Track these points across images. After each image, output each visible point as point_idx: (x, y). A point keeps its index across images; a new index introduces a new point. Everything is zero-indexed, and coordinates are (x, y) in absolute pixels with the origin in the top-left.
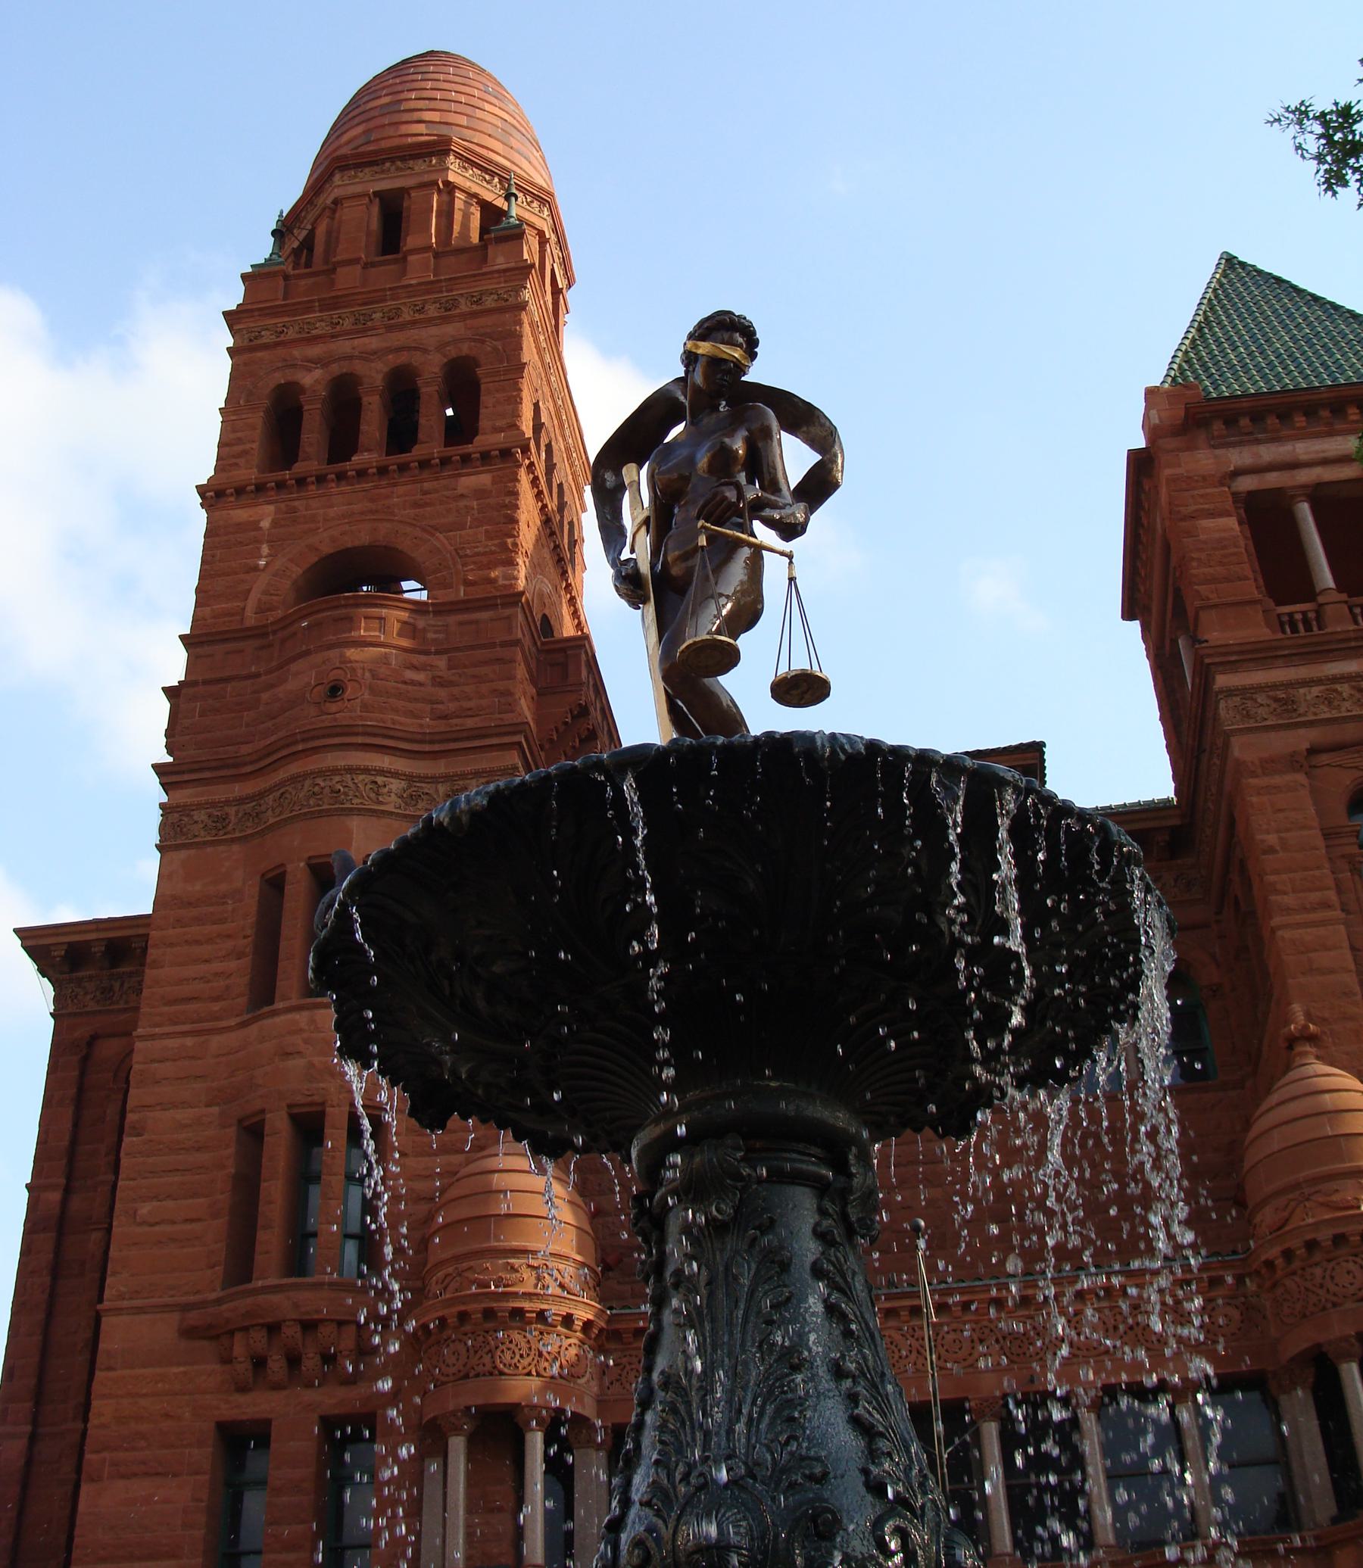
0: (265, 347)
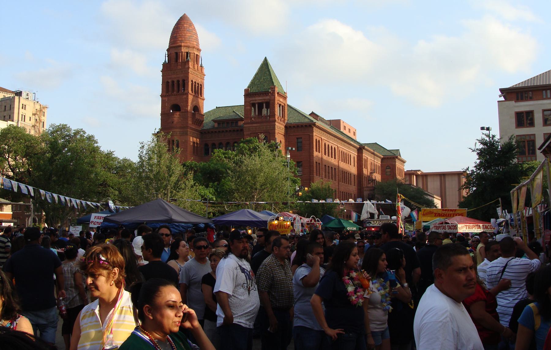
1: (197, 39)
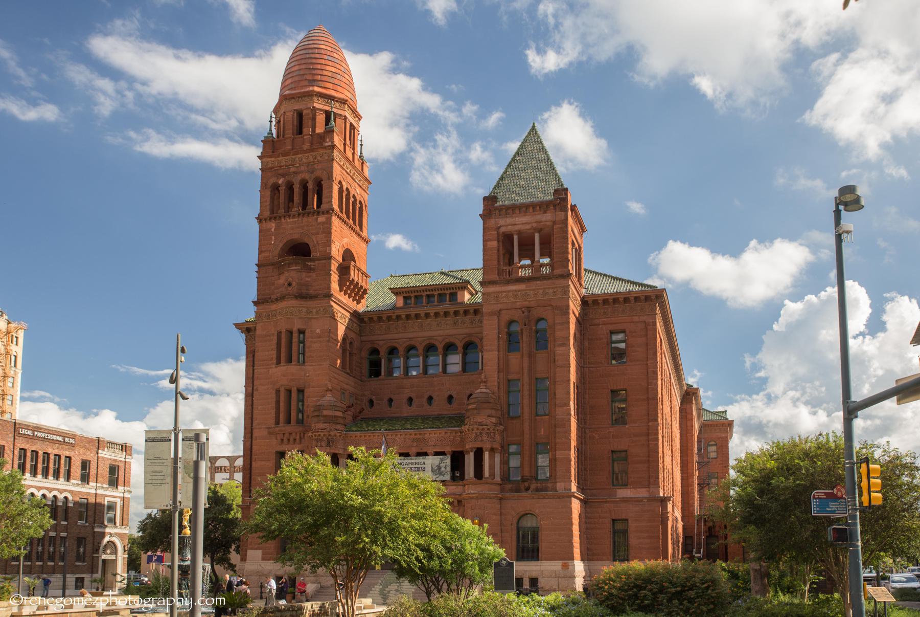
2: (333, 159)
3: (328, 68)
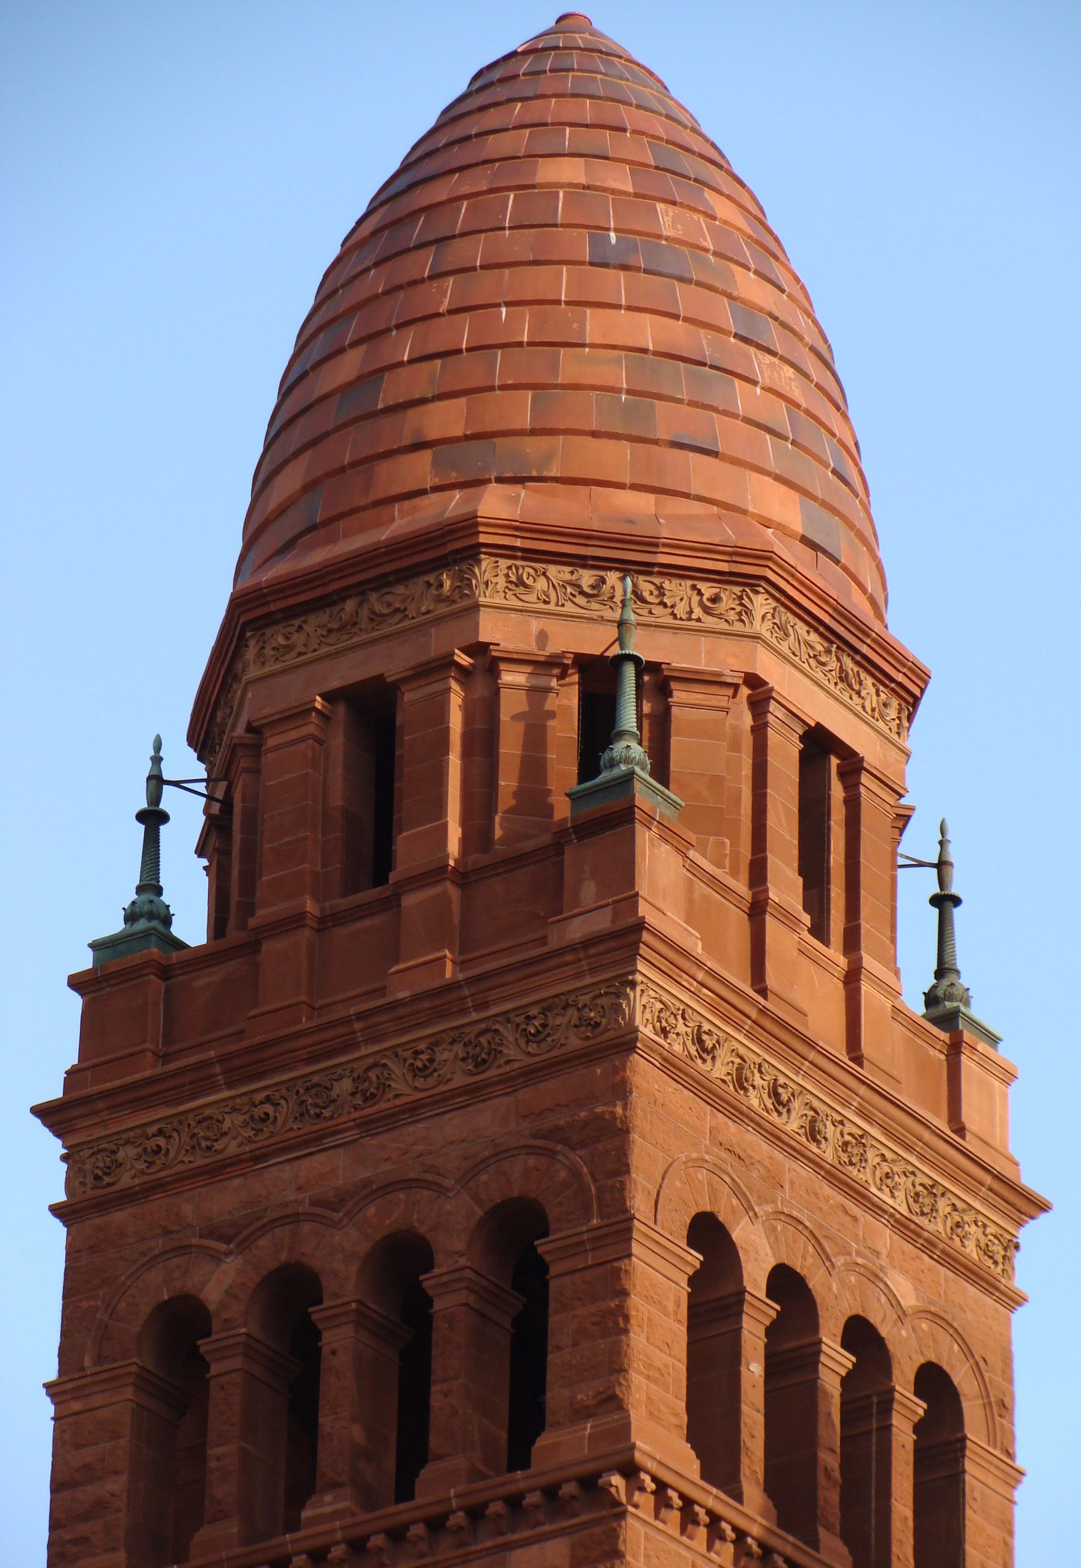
0: (127, 1197)
1: (819, 436)
2: (626, 1043)
3: (594, 325)
